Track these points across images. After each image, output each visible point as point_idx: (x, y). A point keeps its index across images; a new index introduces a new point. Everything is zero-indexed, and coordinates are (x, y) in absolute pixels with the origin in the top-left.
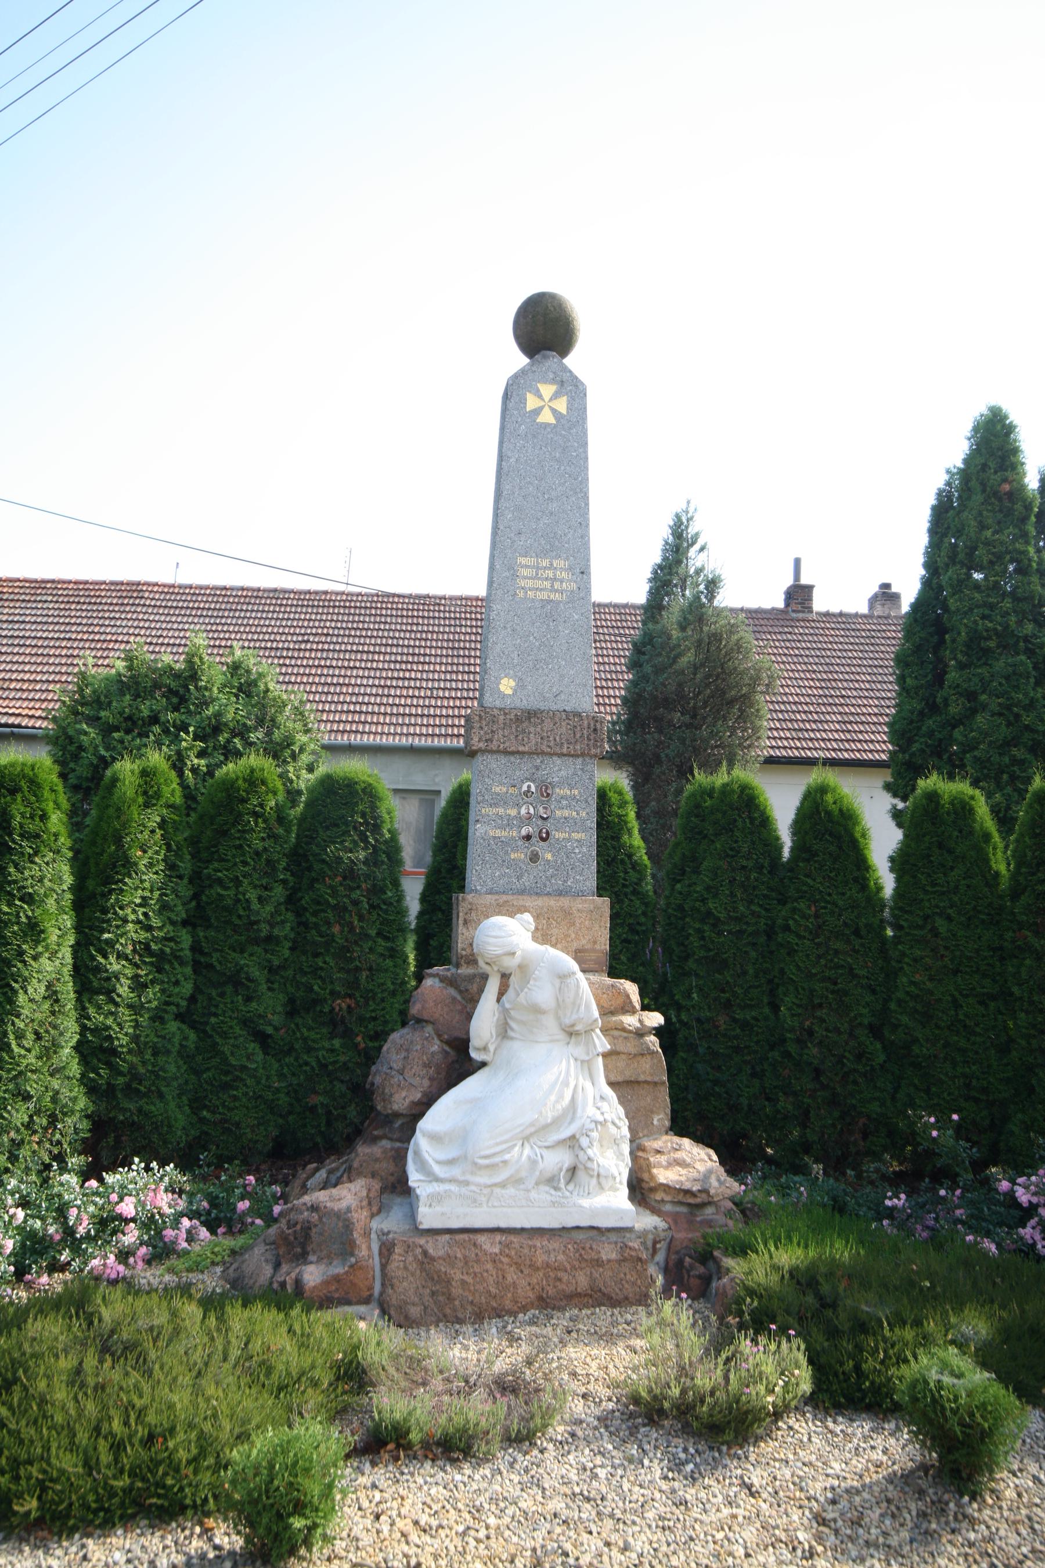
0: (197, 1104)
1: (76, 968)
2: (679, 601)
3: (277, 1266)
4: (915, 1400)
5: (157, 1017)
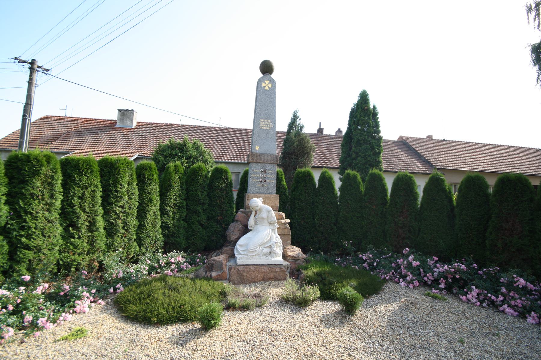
0: (187, 239)
1: (160, 209)
2: (294, 131)
3: (206, 272)
4: (341, 297)
5: (178, 220)
